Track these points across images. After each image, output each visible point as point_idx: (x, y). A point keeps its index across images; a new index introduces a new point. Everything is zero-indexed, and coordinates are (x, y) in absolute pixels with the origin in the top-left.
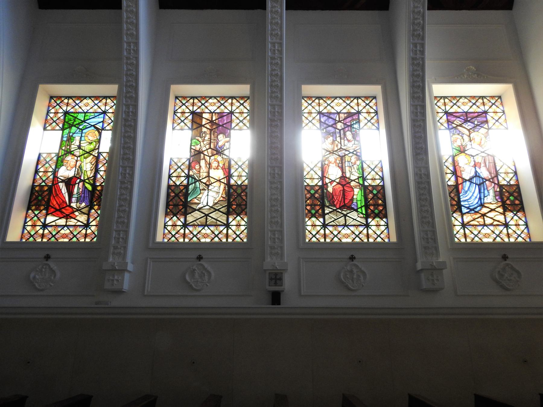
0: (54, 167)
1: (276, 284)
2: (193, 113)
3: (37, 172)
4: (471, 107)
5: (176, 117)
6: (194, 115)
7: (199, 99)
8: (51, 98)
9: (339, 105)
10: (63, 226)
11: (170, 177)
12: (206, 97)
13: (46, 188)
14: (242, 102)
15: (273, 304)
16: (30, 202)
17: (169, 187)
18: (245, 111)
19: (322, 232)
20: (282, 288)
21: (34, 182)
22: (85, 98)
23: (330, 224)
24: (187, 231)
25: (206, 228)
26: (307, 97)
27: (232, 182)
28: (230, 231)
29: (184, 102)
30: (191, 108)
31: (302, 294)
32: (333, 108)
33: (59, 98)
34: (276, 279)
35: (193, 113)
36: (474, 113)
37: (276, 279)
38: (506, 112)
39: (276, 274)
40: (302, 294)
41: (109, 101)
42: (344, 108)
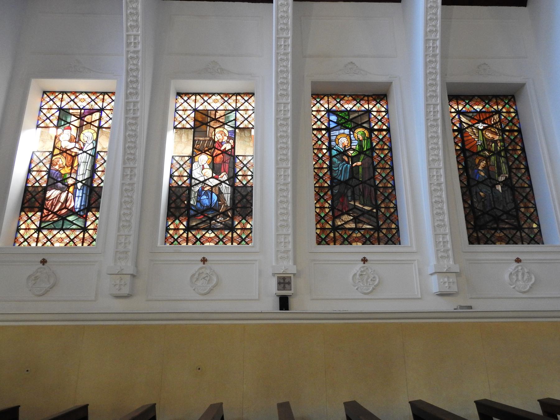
0: (48, 166)
1: (284, 288)
2: (60, 109)
3: (30, 171)
4: (355, 105)
5: (42, 114)
6: (196, 112)
7: (110, 95)
8: (45, 92)
9: (215, 101)
10: (353, 230)
11: (171, 176)
12: (76, 92)
13: (40, 189)
14: (246, 98)
15: (280, 310)
16: (23, 203)
17: (170, 188)
18: (251, 108)
19: (35, 235)
20: (292, 292)
21: (27, 183)
22: (213, 94)
23: (47, 227)
24: (480, 235)
25: (210, 232)
26: (71, 92)
27: (238, 183)
28: (235, 235)
29: (226, 99)
30: (193, 105)
31: (257, 298)
32: (76, 104)
33: (53, 92)
34: (284, 283)
35: (60, 109)
36: (358, 111)
37: (284, 283)
38: (389, 112)
39: (284, 278)
40: (257, 298)
41: (239, 98)
42: (88, 104)
